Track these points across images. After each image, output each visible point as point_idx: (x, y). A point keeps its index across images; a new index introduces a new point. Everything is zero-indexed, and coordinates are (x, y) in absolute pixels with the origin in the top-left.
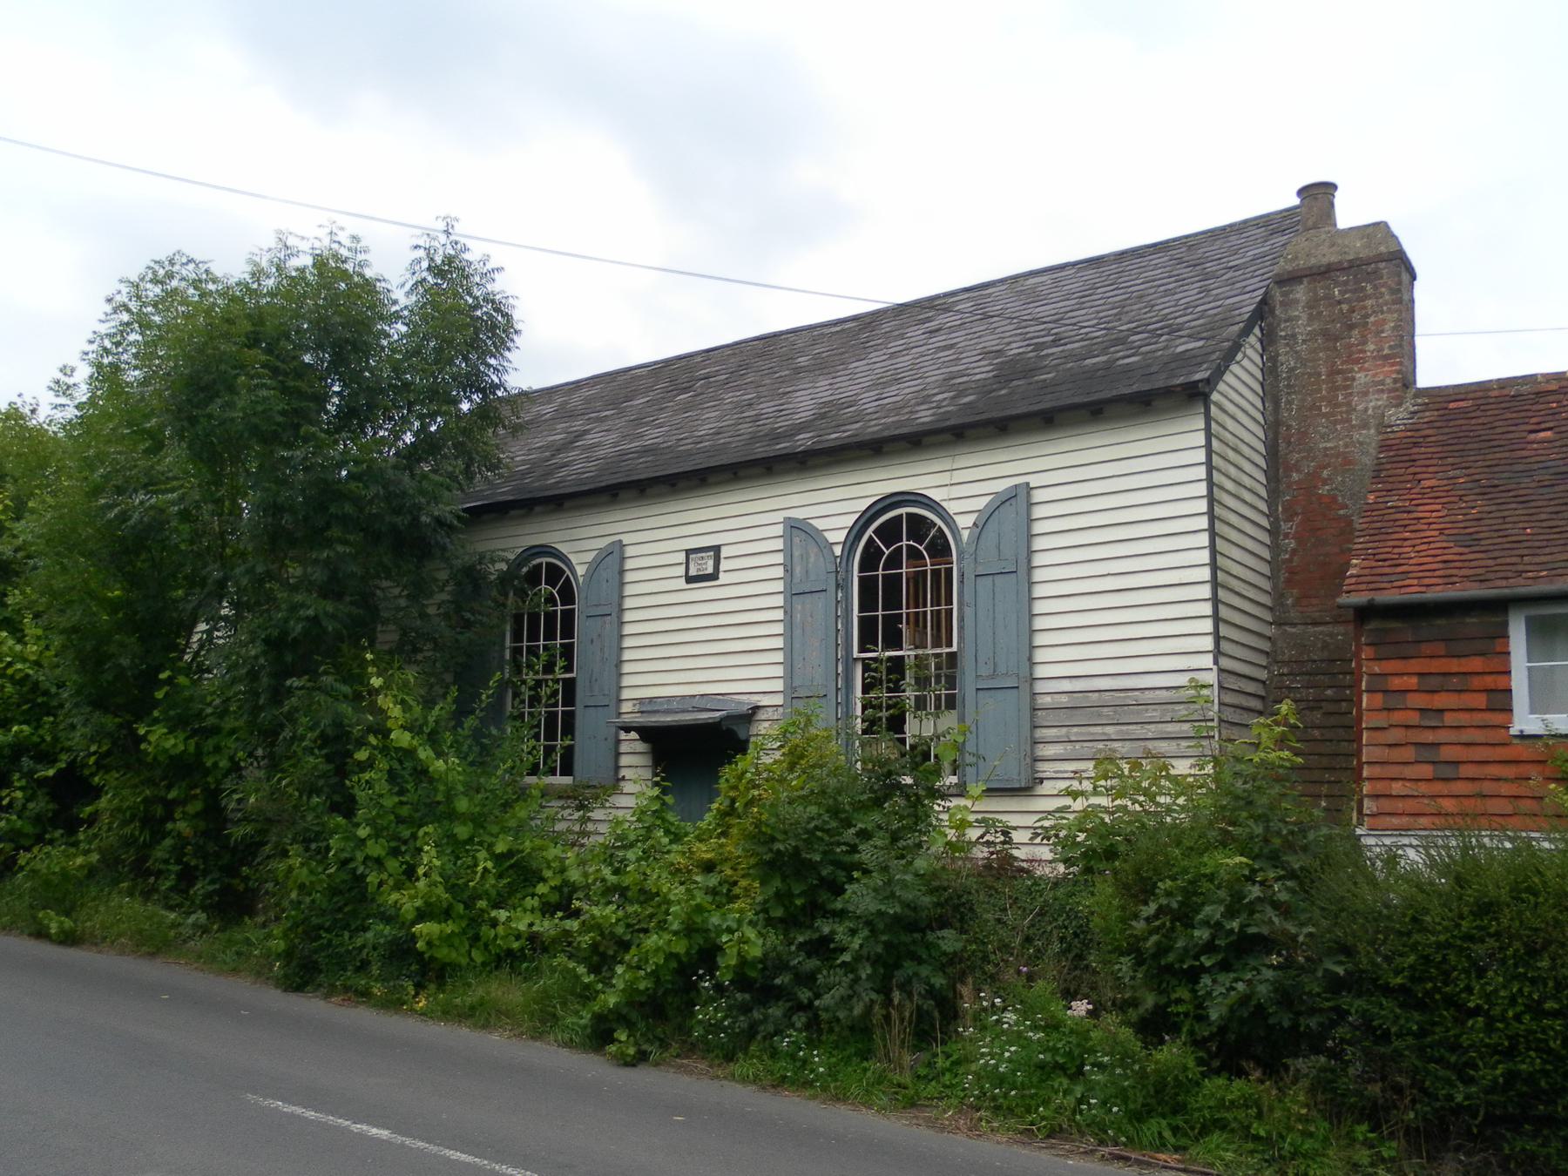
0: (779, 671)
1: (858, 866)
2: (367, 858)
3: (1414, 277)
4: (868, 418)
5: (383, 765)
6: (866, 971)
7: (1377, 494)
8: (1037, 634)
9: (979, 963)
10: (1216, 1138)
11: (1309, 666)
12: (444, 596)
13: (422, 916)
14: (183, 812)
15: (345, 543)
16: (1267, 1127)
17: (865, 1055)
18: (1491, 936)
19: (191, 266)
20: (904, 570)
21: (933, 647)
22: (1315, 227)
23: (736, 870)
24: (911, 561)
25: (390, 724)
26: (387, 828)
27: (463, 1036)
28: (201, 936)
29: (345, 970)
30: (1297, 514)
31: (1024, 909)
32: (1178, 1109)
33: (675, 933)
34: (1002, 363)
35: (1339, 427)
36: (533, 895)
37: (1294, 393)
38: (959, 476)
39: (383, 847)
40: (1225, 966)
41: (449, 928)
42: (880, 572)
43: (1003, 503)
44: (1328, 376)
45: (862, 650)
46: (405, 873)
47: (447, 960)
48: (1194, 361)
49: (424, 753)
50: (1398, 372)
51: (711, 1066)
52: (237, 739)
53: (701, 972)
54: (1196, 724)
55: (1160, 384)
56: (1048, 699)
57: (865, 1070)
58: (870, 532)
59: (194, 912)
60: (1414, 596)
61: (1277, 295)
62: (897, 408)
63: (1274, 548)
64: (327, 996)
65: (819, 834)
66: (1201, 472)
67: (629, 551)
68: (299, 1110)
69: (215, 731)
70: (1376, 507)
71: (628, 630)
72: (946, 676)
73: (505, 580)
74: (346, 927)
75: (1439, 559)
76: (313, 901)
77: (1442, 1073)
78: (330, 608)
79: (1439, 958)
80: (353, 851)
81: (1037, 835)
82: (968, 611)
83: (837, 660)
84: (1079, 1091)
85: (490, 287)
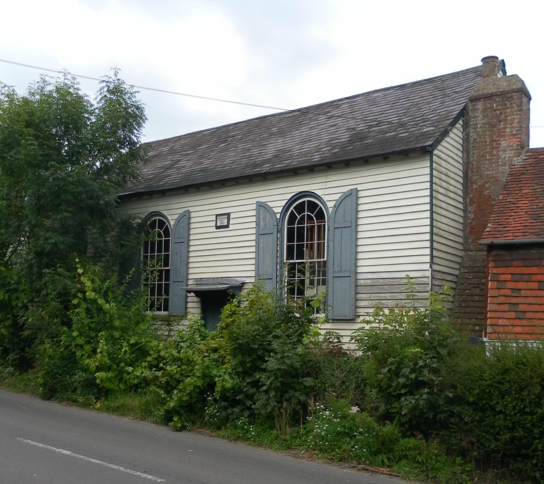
0: (253, 268)
1: (273, 351)
2: (76, 345)
3: (529, 98)
4: (294, 158)
5: (84, 305)
6: (272, 394)
7: (504, 195)
8: (190, 275)
9: (322, 391)
10: (403, 462)
11: (476, 269)
12: (114, 233)
13: (98, 369)
14: (4, 325)
15: (66, 211)
16: (422, 458)
17: (272, 428)
18: (507, 382)
19: (6, 88)
20: (305, 225)
21: (318, 258)
22: (488, 76)
23: (226, 352)
24: (309, 221)
25: (86, 289)
26: (85, 332)
27: (114, 419)
28: (11, 377)
29: (67, 391)
30: (474, 203)
31: (343, 370)
32: (391, 450)
33: (198, 377)
34: (353, 134)
35: (493, 165)
36: (146, 361)
37: (476, 150)
38: (329, 185)
39: (83, 340)
40: (411, 393)
41: (110, 374)
42: (296, 226)
43: (346, 197)
44: (490, 142)
45: (288, 259)
46: (92, 351)
47: (109, 388)
48: (429, 136)
49: (101, 301)
50: (519, 141)
51: (211, 432)
52: (25, 294)
53: (209, 393)
54: (407, 294)
55: (412, 147)
56: (362, 282)
57: (271, 434)
58: (292, 208)
59: (8, 367)
60: (509, 241)
61: (470, 106)
62: (306, 154)
63: (465, 217)
64: (60, 402)
65: (258, 337)
66: (428, 185)
67: (193, 215)
68: (36, 444)
69: (16, 290)
70: (502, 201)
71: (191, 249)
72: (322, 271)
73: (141, 226)
74: (68, 374)
75: (522, 225)
76: (55, 363)
77: (488, 436)
78: (61, 240)
79: (488, 391)
80: (70, 342)
81: (352, 339)
82: (331, 243)
83: (277, 263)
84: (353, 443)
85: (134, 100)
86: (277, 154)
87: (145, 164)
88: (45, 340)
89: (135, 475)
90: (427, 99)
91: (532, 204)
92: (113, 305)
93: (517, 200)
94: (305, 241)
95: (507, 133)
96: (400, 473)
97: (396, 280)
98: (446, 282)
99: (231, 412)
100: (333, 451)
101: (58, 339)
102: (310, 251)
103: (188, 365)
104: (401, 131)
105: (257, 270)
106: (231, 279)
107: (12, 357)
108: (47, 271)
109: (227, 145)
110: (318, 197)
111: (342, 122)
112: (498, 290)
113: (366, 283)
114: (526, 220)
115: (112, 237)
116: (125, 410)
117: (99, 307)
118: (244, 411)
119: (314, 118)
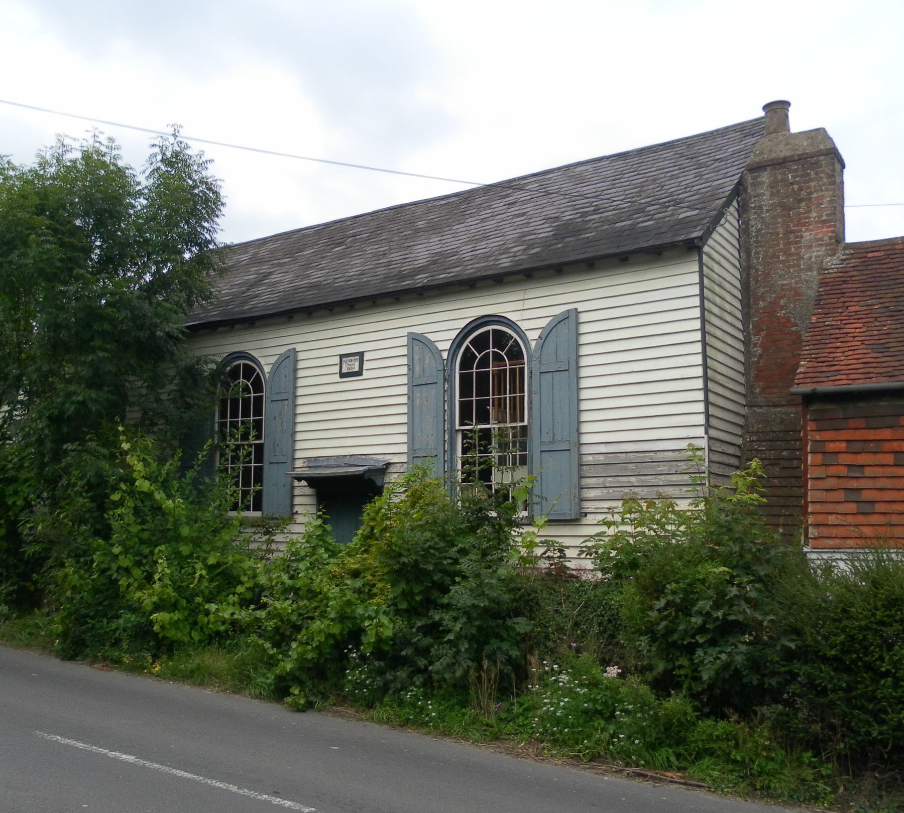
0: (404, 438)
1: (459, 573)
2: (119, 568)
3: (843, 166)
4: (466, 263)
5: (130, 503)
6: (464, 646)
7: (818, 316)
9: (543, 640)
10: (707, 761)
13: (157, 608)
16: (742, 754)
17: (464, 704)
22: (775, 131)
23: (374, 576)
25: (135, 475)
26: (133, 547)
27: (185, 691)
28: (4, 622)
30: (763, 330)
32: (680, 741)
33: (332, 620)
34: (558, 226)
36: (234, 594)
38: (529, 304)
39: (131, 561)
40: (713, 643)
41: (176, 616)
42: (474, 370)
43: (559, 322)
44: (784, 234)
45: (462, 424)
46: (145, 578)
47: (175, 639)
49: (159, 496)
50: (833, 232)
51: (357, 712)
52: (29, 486)
53: (350, 647)
54: (693, 475)
55: (668, 240)
56: (590, 458)
57: (464, 714)
58: (467, 342)
61: (749, 180)
62: (486, 257)
63: (747, 353)
64: (92, 664)
65: (432, 551)
66: (696, 301)
67: (301, 356)
68: (72, 742)
69: (13, 480)
71: (300, 410)
72: (520, 442)
73: (215, 376)
74: (105, 615)
75: (861, 361)
76: (82, 598)
77: (863, 716)
78: (94, 396)
79: (861, 637)
80: (109, 563)
81: (583, 552)
82: (535, 398)
83: (445, 431)
85: (204, 173)
86: (435, 258)
87: (220, 277)
88: (65, 561)
89: (259, 799)
90: (670, 172)
91: (869, 329)
92: (179, 502)
93: (843, 322)
94: (491, 394)
95: (812, 219)
96: (703, 780)
97: (647, 454)
98: (726, 456)
99: (392, 678)
100: (577, 743)
101: (87, 558)
102: (498, 411)
103: (309, 599)
104: (641, 219)
105: (411, 442)
106: (367, 457)
107: (6, 588)
108: (68, 446)
109: (347, 248)
110: (512, 325)
111: (533, 210)
112: (824, 468)
113: (597, 461)
114: (865, 354)
115: (169, 394)
116: (204, 676)
117: (155, 506)
118: (414, 676)
119: (485, 205)
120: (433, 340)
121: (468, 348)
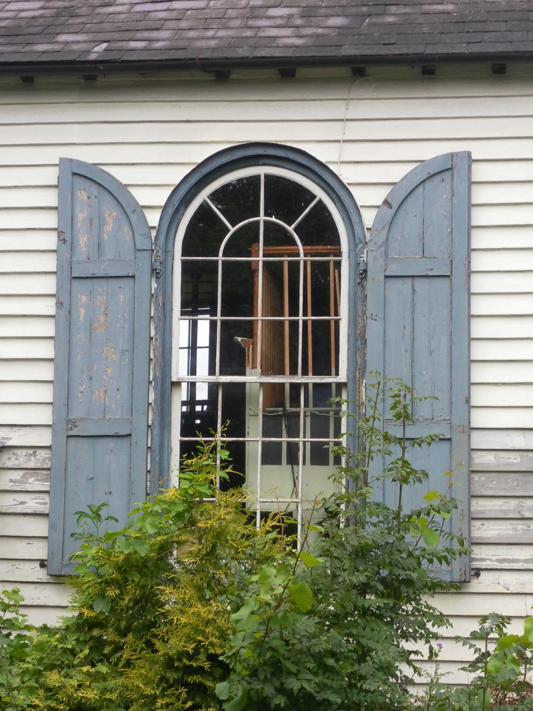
42: (220, 258)
43: (431, 177)
58: (204, 196)
120: (124, 182)
121: (204, 209)
